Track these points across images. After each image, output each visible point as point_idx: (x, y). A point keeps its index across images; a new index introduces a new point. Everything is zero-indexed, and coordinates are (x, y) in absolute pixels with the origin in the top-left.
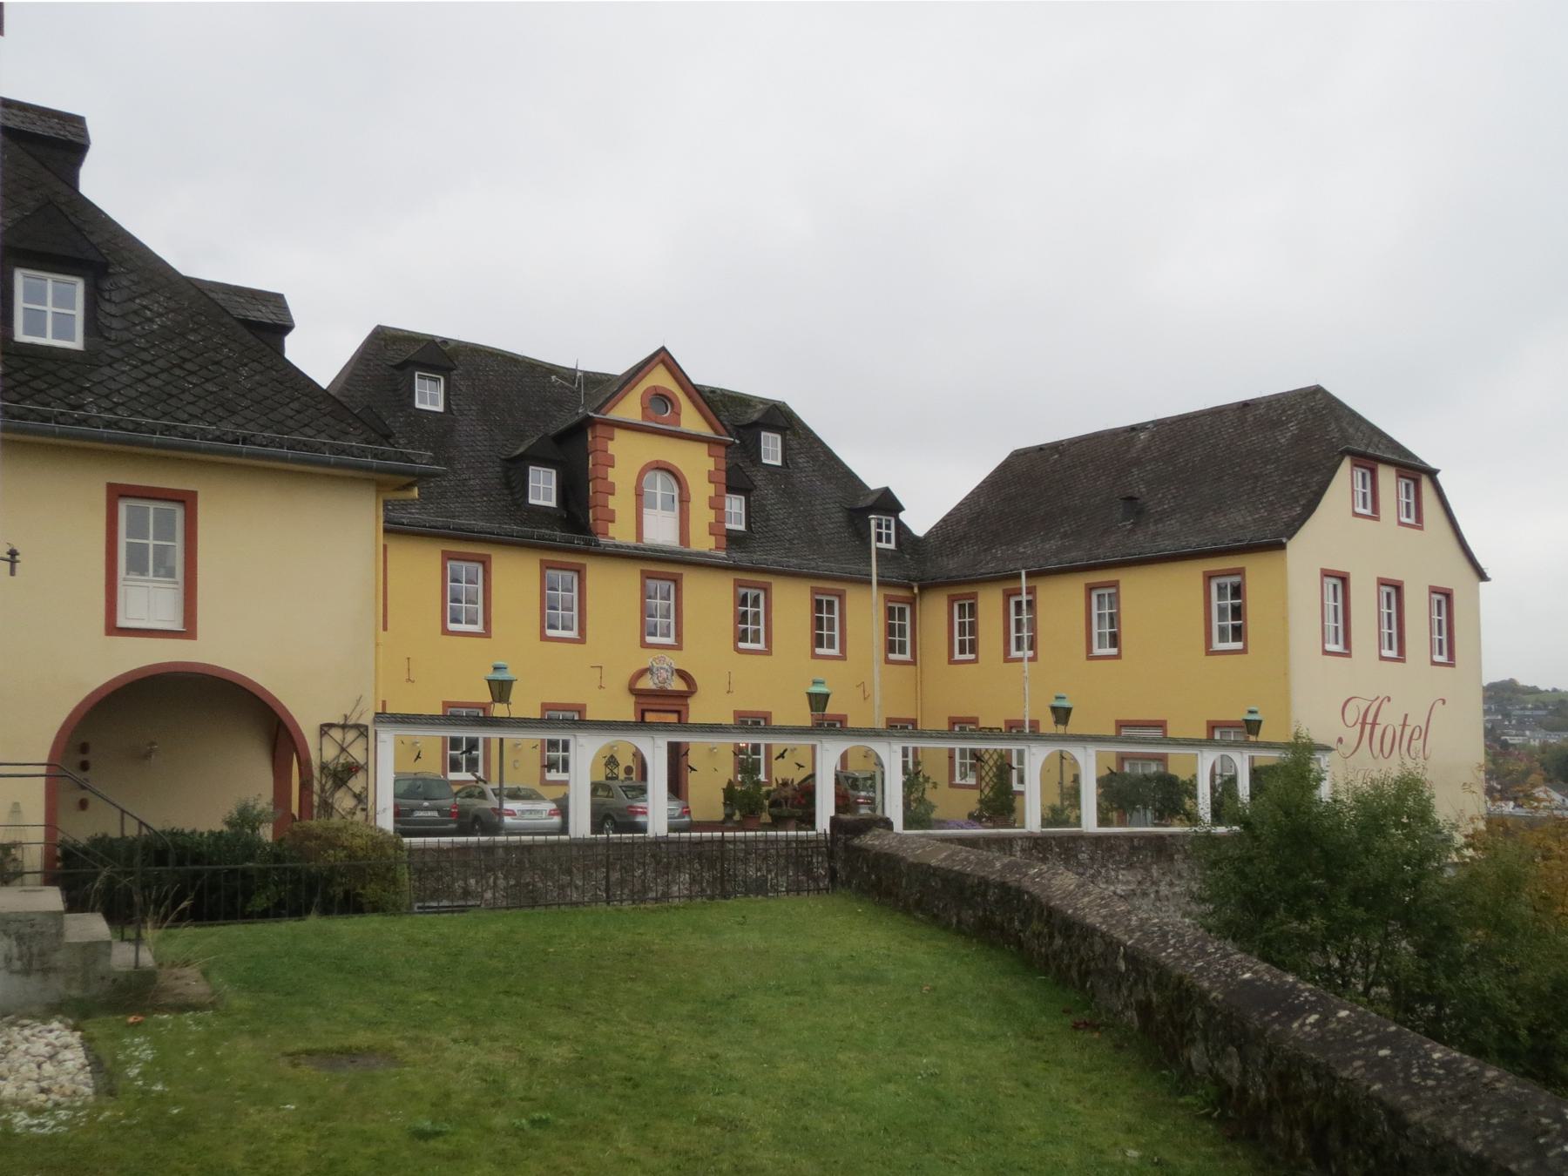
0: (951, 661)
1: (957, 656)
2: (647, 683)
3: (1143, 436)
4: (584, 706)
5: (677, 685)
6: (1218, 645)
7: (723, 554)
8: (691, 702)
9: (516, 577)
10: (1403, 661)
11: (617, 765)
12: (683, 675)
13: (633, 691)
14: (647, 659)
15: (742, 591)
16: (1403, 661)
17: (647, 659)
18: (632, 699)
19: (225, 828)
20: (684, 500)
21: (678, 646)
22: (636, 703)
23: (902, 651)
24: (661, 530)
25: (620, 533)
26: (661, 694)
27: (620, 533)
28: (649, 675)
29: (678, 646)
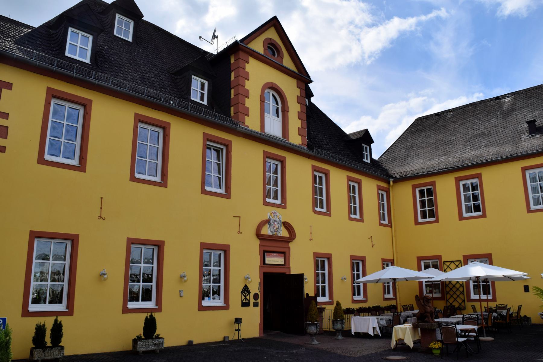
0: (417, 223)
1: (420, 220)
2: (266, 231)
3: (507, 100)
4: (229, 246)
5: (284, 233)
6: (465, 215)
7: (306, 148)
8: (291, 245)
9: (187, 139)
10: (84, 170)
11: (249, 293)
12: (287, 226)
13: (259, 235)
14: (267, 213)
15: (315, 173)
16: (84, 170)
17: (267, 213)
18: (258, 242)
19: (391, 46)
20: (285, 111)
21: (283, 206)
22: (260, 245)
23: (276, 198)
24: (273, 127)
25: (252, 123)
26: (274, 239)
27: (252, 123)
28: (267, 226)
29: (283, 206)
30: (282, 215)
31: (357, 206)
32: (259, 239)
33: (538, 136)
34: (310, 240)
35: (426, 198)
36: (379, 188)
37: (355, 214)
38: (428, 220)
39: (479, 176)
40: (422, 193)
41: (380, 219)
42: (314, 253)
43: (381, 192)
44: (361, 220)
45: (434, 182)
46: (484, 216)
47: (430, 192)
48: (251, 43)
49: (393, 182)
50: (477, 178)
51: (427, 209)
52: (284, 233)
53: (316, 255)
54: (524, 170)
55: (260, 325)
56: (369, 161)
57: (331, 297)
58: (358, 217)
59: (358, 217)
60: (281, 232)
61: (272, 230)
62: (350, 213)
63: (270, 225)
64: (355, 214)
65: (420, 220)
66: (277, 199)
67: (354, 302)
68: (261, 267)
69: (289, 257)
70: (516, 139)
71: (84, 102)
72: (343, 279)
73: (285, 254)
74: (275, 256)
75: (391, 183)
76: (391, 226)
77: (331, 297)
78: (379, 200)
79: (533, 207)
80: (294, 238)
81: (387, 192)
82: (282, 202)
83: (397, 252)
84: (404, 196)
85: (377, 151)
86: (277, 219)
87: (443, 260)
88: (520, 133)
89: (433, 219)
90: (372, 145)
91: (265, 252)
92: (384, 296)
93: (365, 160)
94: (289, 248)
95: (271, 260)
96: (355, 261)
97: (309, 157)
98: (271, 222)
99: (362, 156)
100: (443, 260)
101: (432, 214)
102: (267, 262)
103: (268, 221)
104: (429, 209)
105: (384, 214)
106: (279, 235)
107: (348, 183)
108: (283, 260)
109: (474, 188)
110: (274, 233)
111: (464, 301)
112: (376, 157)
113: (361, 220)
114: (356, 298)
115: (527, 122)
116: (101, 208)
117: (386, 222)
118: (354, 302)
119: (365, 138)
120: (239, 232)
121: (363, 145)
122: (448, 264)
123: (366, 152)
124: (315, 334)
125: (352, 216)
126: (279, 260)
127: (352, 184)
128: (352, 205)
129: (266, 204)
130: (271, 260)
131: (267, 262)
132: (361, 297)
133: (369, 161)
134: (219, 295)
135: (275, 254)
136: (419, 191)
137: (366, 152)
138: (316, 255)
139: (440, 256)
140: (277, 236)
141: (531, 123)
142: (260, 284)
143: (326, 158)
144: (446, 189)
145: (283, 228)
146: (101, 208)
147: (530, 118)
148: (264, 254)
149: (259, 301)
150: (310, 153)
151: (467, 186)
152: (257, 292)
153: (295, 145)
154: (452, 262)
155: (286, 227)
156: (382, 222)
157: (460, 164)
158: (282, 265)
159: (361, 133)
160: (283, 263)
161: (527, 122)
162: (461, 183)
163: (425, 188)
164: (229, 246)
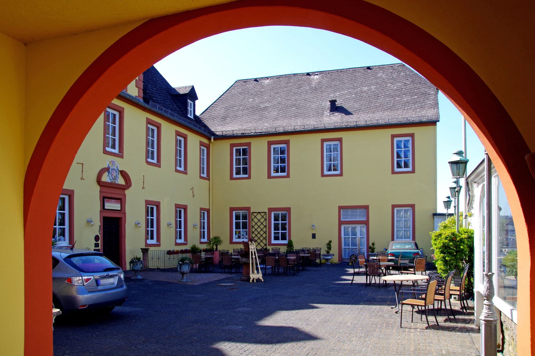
0: (232, 178)
2: (105, 178)
5: (121, 181)
7: (142, 100)
8: (127, 192)
13: (99, 181)
14: (106, 161)
15: (149, 126)
17: (106, 161)
18: (98, 188)
21: (120, 155)
29: (120, 155)
30: (120, 164)
31: (155, 150)
32: (100, 185)
33: (336, 114)
34: (143, 188)
35: (241, 157)
36: (202, 144)
37: (153, 159)
38: (242, 176)
39: (287, 142)
40: (238, 151)
41: (176, 166)
42: (176, 204)
43: (202, 148)
44: (185, 172)
45: (250, 143)
46: (288, 176)
47: (245, 152)
49: (214, 139)
50: (286, 143)
51: (241, 166)
52: (121, 181)
53: (147, 202)
54: (323, 141)
56: (192, 117)
57: (186, 239)
58: (155, 161)
59: (155, 161)
60: (118, 180)
61: (111, 178)
62: (147, 157)
63: (109, 173)
64: (153, 159)
65: (235, 176)
66: (115, 148)
67: (177, 244)
68: (101, 212)
69: (125, 203)
70: (319, 113)
71: (120, 110)
72: (89, 222)
73: (121, 200)
74: (112, 202)
75: (212, 140)
76: (209, 180)
77: (186, 239)
78: (176, 146)
79: (326, 173)
80: (130, 186)
81: (207, 148)
82: (120, 152)
83: (212, 203)
84: (222, 152)
85: (200, 107)
86: (115, 168)
87: (252, 211)
88: (323, 110)
89: (246, 176)
90: (196, 101)
91: (104, 198)
92: (146, 242)
93: (189, 116)
94: (125, 195)
95: (109, 205)
96: (150, 206)
97: (144, 109)
98: (110, 170)
99: (187, 113)
100: (252, 211)
101: (245, 171)
102: (106, 208)
103: (107, 169)
104: (243, 168)
105: (180, 160)
106: (117, 183)
107: (176, 137)
108: (120, 205)
109: (282, 152)
110: (113, 181)
111: (266, 245)
112: (198, 113)
113: (185, 172)
114: (150, 242)
115: (330, 101)
117: (182, 169)
118: (177, 244)
119: (192, 95)
120: (82, 178)
121: (188, 100)
122: (255, 214)
123: (191, 108)
124: (140, 271)
125: (150, 160)
126: (117, 207)
127: (150, 126)
128: (150, 149)
129: (105, 152)
130: (109, 205)
131: (106, 208)
132: (182, 241)
133: (192, 117)
134: (64, 236)
135: (113, 200)
136: (236, 149)
137: (191, 108)
138: (147, 202)
139: (250, 208)
140: (115, 184)
141: (333, 102)
142: (100, 226)
143: (160, 112)
144: (259, 152)
147: (332, 97)
148: (104, 199)
149: (99, 242)
150: (146, 106)
151: (276, 150)
152: (98, 234)
153: (133, 97)
154: (259, 213)
155: (122, 175)
156: (178, 168)
157: (273, 130)
158: (119, 210)
159: (187, 89)
160: (120, 209)
161: (330, 101)
162: (273, 147)
163: (242, 148)
164: (73, 191)
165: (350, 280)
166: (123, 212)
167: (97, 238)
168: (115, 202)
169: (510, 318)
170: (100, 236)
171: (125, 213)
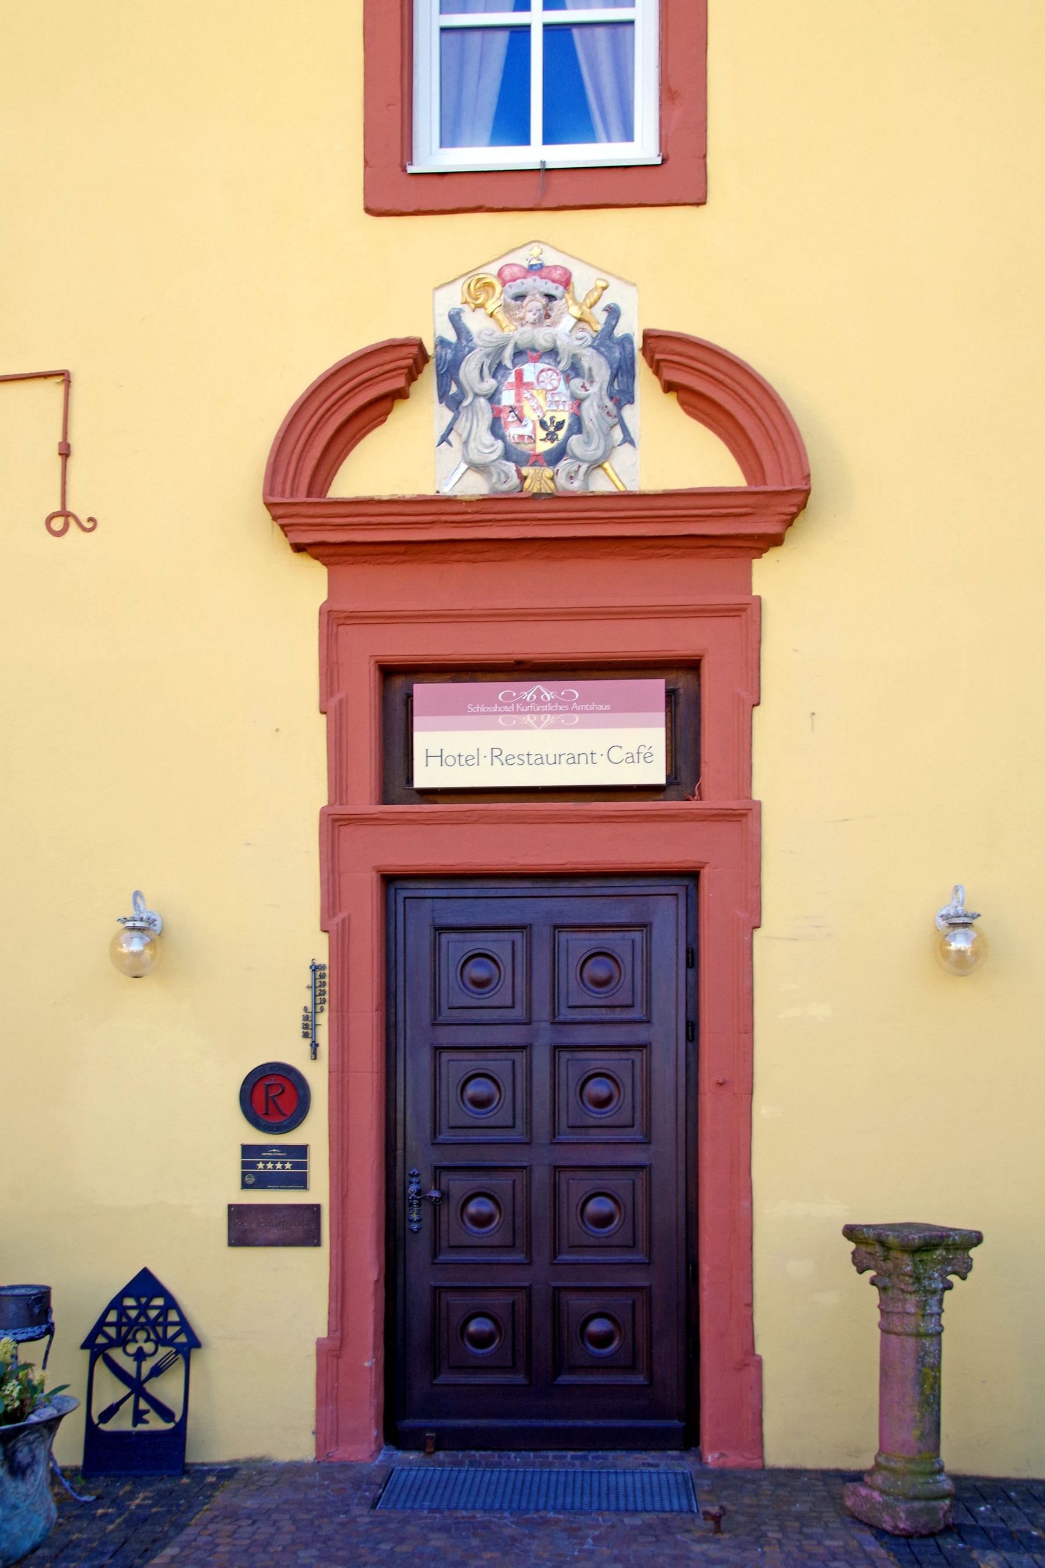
2: (405, 460)
5: (670, 453)
8: (769, 576)
12: (704, 379)
13: (302, 500)
14: (421, 279)
17: (421, 279)
30: (637, 271)
48: (334, 483)
55: (331, 1354)
63: (454, 402)
68: (335, 824)
73: (697, 699)
74: (522, 708)
86: (563, 330)
91: (397, 678)
94: (746, 613)
95: (458, 747)
98: (469, 370)
108: (653, 737)
116: (65, 452)
126: (621, 745)
130: (458, 747)
145: (652, 408)
146: (65, 452)
148: (382, 700)
152: (293, 1053)
165: (642, 1479)
166: (714, 794)
167: (272, 1095)
168: (565, 707)
169: (100, 1366)
170: (317, 1076)
171: (743, 817)
